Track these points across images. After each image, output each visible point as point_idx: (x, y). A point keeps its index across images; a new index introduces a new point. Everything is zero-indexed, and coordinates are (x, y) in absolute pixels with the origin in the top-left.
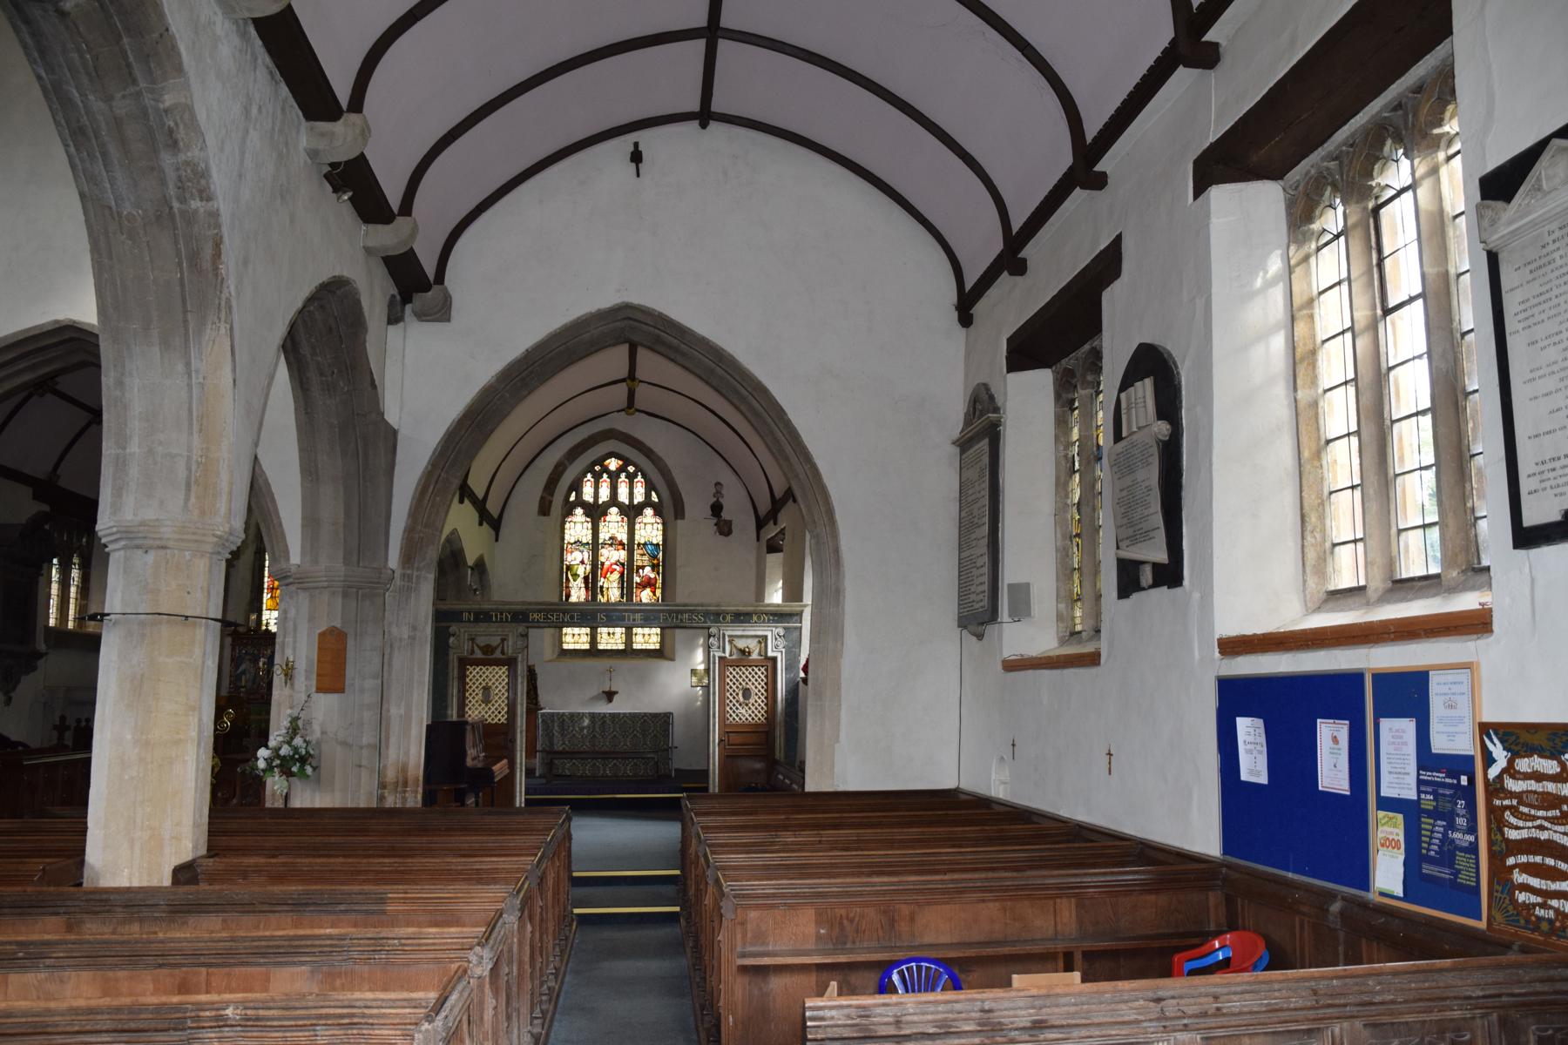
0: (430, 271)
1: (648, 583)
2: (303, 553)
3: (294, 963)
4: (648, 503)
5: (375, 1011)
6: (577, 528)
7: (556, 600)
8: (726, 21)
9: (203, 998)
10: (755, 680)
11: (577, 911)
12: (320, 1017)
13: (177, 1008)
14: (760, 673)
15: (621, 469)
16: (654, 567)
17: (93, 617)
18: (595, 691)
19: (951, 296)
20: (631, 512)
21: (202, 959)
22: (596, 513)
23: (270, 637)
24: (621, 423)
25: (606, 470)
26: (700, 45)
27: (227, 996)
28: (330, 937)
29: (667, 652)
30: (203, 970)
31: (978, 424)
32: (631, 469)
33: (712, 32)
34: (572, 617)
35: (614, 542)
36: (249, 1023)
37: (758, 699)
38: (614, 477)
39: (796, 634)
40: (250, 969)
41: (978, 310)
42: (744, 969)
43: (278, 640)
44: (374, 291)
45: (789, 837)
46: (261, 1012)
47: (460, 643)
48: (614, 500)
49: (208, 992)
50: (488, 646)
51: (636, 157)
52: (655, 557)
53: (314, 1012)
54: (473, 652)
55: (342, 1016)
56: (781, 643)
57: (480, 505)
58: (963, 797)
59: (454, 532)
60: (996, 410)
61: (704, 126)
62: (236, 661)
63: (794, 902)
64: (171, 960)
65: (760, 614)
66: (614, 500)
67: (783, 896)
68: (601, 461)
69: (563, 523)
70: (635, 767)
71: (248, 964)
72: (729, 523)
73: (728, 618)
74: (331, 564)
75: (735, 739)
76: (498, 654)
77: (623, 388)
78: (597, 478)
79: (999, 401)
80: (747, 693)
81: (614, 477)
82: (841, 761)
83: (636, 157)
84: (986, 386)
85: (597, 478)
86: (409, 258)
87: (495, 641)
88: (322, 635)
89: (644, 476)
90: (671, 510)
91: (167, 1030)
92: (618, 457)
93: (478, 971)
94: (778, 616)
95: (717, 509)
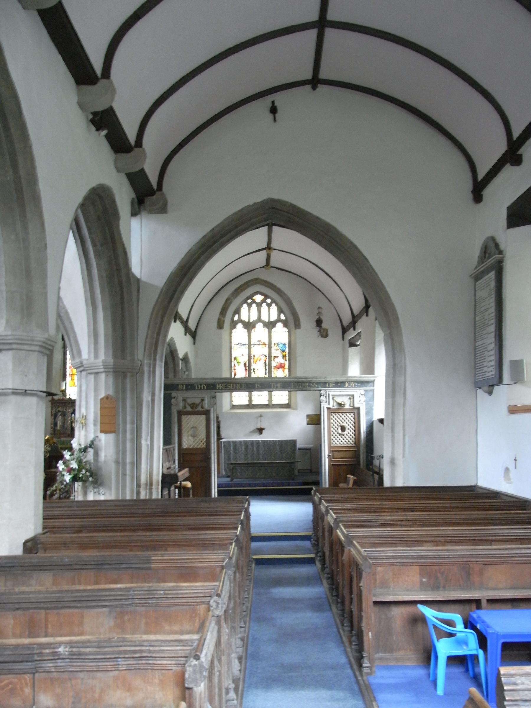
0: (154, 181)
1: (281, 366)
2: (89, 353)
3: (98, 607)
4: (279, 320)
5: (157, 648)
6: (239, 334)
7: (228, 376)
8: (332, 15)
9: (43, 640)
10: (348, 421)
11: (254, 557)
12: (120, 652)
13: (28, 647)
14: (351, 416)
15: (264, 301)
16: (284, 357)
17: (333, 589)
18: (253, 427)
19: (469, 186)
20: (270, 325)
21: (42, 605)
22: (249, 326)
23: (72, 403)
24: (264, 275)
25: (254, 302)
26: (313, 34)
27: (59, 639)
28: (120, 589)
29: (292, 405)
30: (43, 612)
31: (489, 262)
32: (269, 301)
33: (322, 24)
34: (241, 386)
35: (260, 343)
36: (73, 656)
37: (349, 432)
38: (259, 305)
39: (371, 393)
40: (71, 611)
41: (487, 192)
42: (376, 603)
43: (77, 403)
44: (123, 196)
45: (387, 517)
46: (82, 650)
47: (178, 404)
48: (259, 320)
49: (46, 636)
50: (193, 404)
51: (274, 110)
52: (284, 351)
53: (116, 649)
54: (185, 407)
55: (135, 652)
56: (363, 398)
57: (185, 324)
58: (481, 491)
59: (172, 339)
60: (501, 252)
61: (314, 88)
62: (55, 416)
63: (405, 563)
64: (24, 606)
65: (349, 382)
66: (259, 320)
67: (399, 558)
68: (251, 297)
69: (231, 333)
70: (286, 471)
71: (70, 607)
72: (326, 331)
73: (331, 385)
74: (103, 356)
75: (337, 455)
76: (199, 409)
77: (264, 253)
78: (250, 305)
79: (502, 247)
80: (343, 429)
81: (259, 305)
82: (401, 470)
83: (274, 110)
84: (493, 239)
85: (250, 305)
86: (142, 173)
87: (197, 401)
88: (102, 399)
89: (277, 304)
90: (293, 322)
91: (22, 662)
92: (262, 294)
93: (217, 612)
94: (361, 383)
95: (319, 322)
